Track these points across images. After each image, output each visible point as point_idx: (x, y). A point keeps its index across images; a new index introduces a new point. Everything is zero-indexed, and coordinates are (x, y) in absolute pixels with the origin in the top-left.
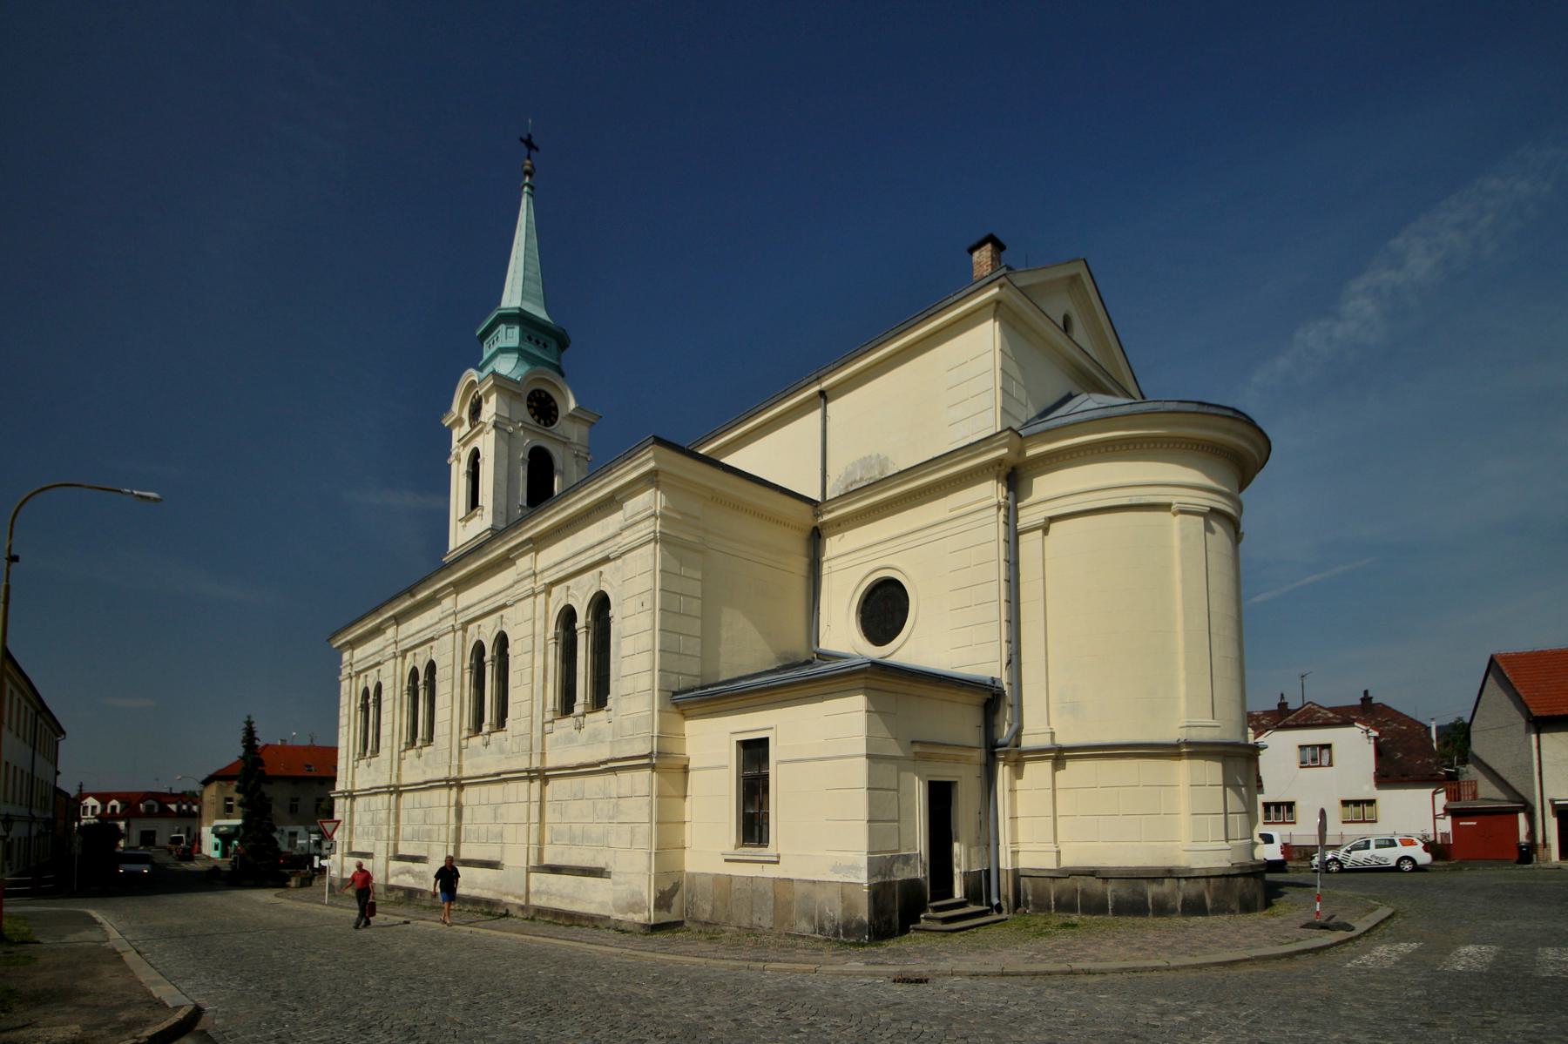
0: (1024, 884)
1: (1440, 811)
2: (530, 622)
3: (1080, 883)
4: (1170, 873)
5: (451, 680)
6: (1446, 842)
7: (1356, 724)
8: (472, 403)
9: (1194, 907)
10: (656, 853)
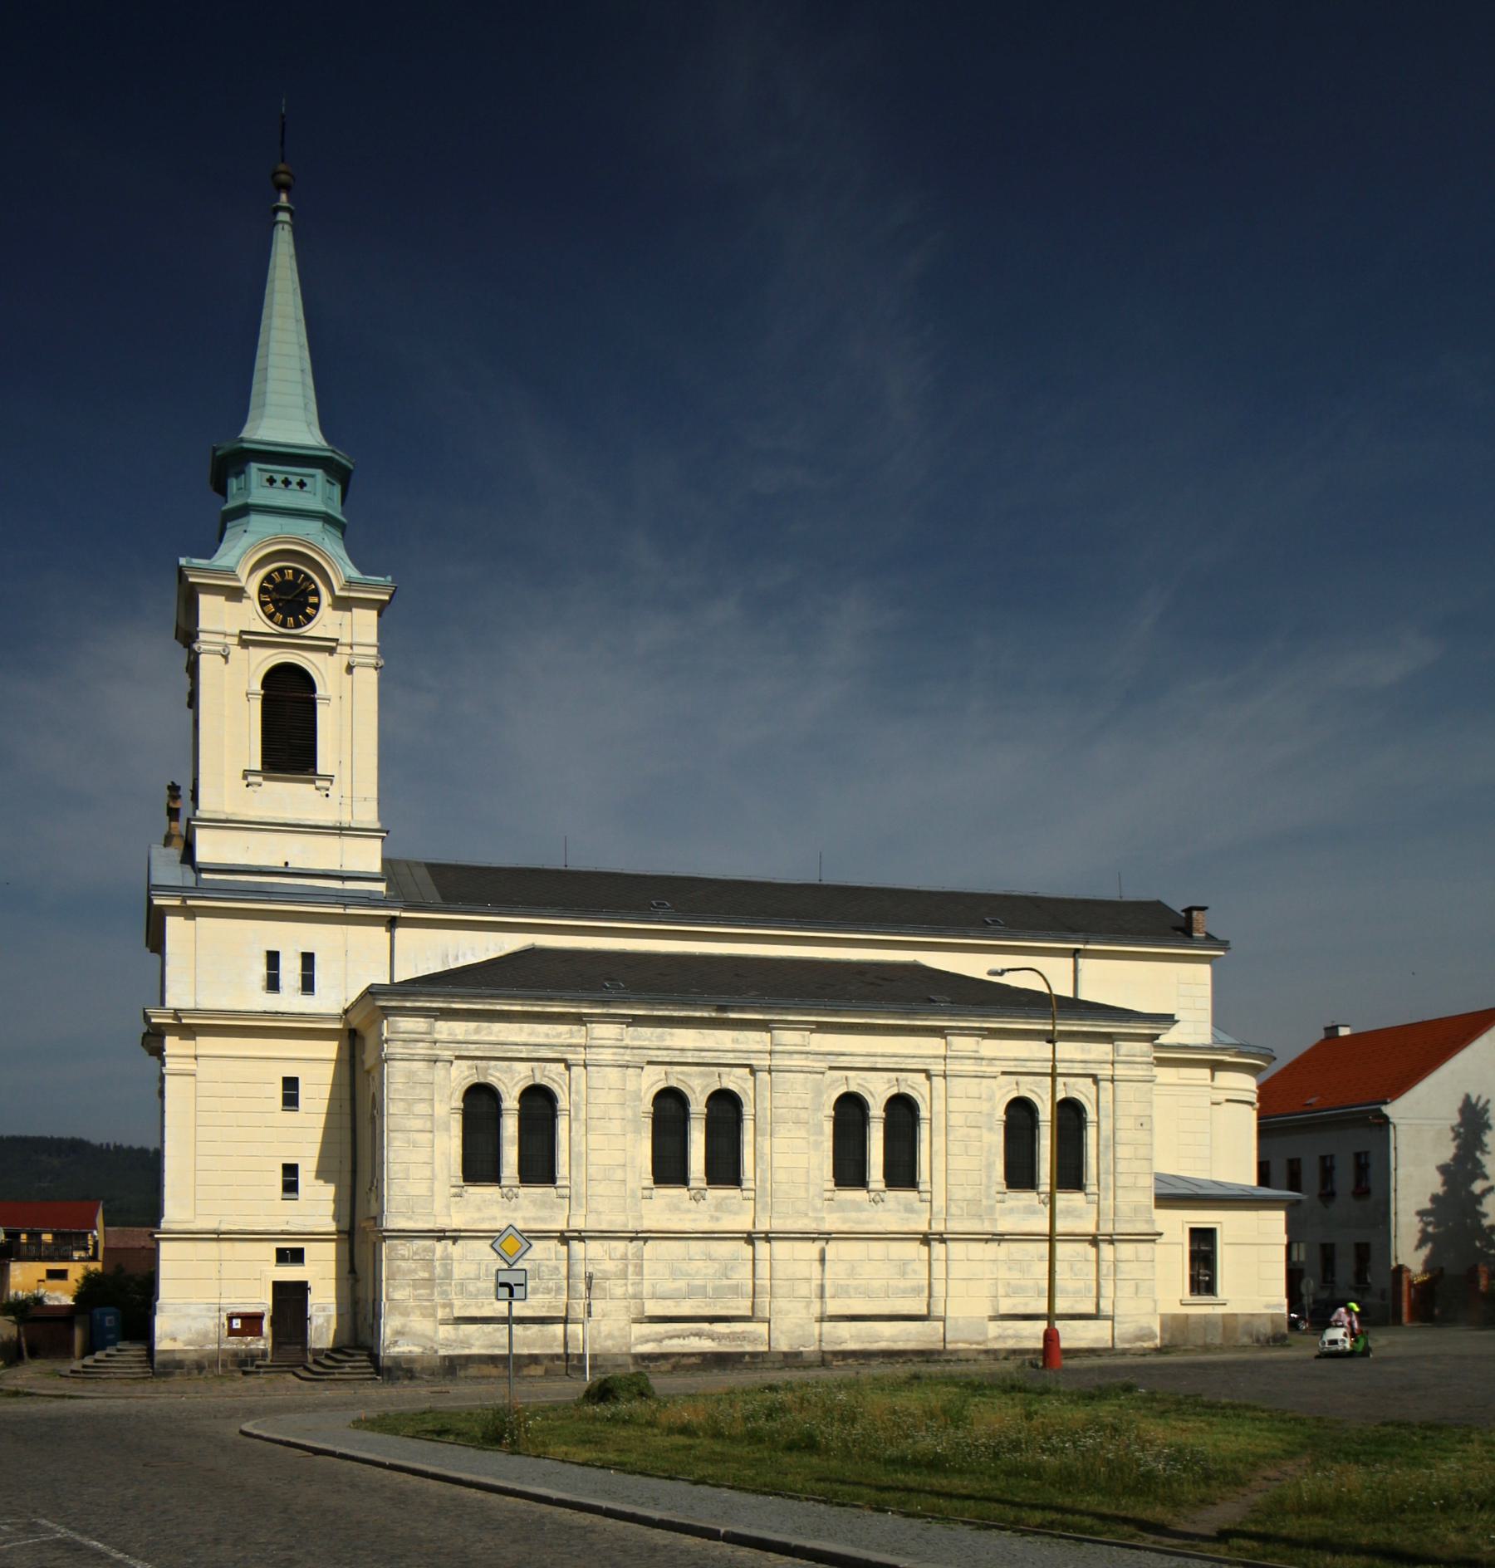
8: (268, 578)
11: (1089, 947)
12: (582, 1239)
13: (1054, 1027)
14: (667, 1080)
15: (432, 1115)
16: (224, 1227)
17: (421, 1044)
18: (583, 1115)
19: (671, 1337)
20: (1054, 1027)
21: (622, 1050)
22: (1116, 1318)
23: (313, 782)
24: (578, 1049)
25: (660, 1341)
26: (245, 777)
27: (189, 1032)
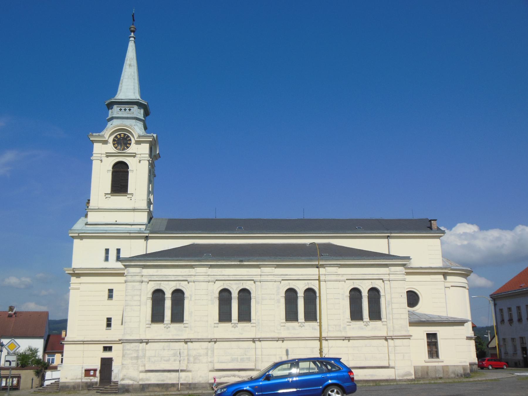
8: (116, 137)
11: (392, 235)
12: (192, 342)
13: (319, 263)
14: (223, 286)
15: (140, 300)
16: (86, 340)
17: (137, 277)
18: (193, 299)
19: (224, 377)
20: (319, 263)
21: (207, 276)
22: (396, 368)
23: (126, 196)
24: (192, 276)
25: (220, 378)
26: (105, 196)
27: (78, 275)
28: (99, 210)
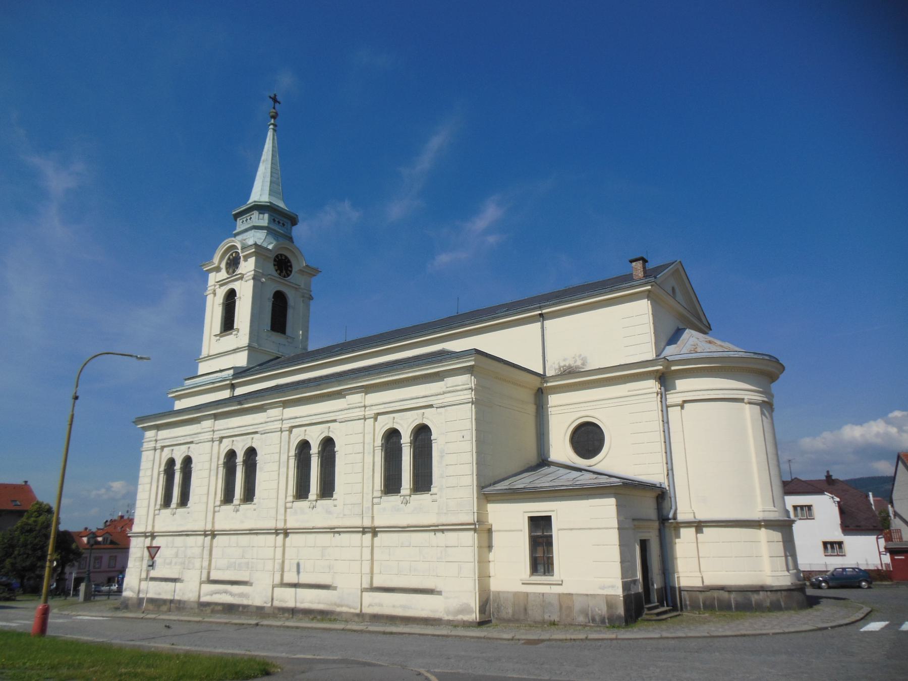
0: (684, 595)
1: (882, 549)
2: (362, 435)
3: (716, 594)
4: (762, 589)
5: (278, 463)
6: (888, 569)
7: (826, 493)
8: (229, 259)
9: (775, 607)
10: (478, 580)
23: (231, 334)
28: (210, 357)
